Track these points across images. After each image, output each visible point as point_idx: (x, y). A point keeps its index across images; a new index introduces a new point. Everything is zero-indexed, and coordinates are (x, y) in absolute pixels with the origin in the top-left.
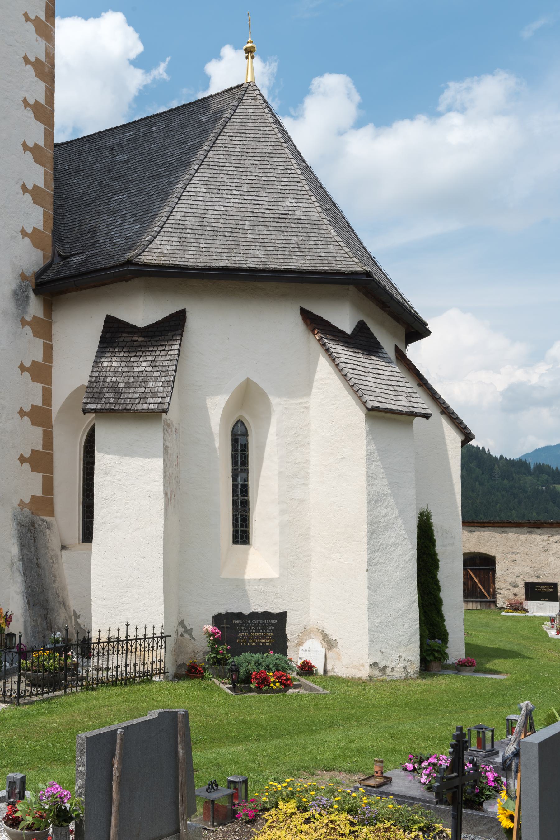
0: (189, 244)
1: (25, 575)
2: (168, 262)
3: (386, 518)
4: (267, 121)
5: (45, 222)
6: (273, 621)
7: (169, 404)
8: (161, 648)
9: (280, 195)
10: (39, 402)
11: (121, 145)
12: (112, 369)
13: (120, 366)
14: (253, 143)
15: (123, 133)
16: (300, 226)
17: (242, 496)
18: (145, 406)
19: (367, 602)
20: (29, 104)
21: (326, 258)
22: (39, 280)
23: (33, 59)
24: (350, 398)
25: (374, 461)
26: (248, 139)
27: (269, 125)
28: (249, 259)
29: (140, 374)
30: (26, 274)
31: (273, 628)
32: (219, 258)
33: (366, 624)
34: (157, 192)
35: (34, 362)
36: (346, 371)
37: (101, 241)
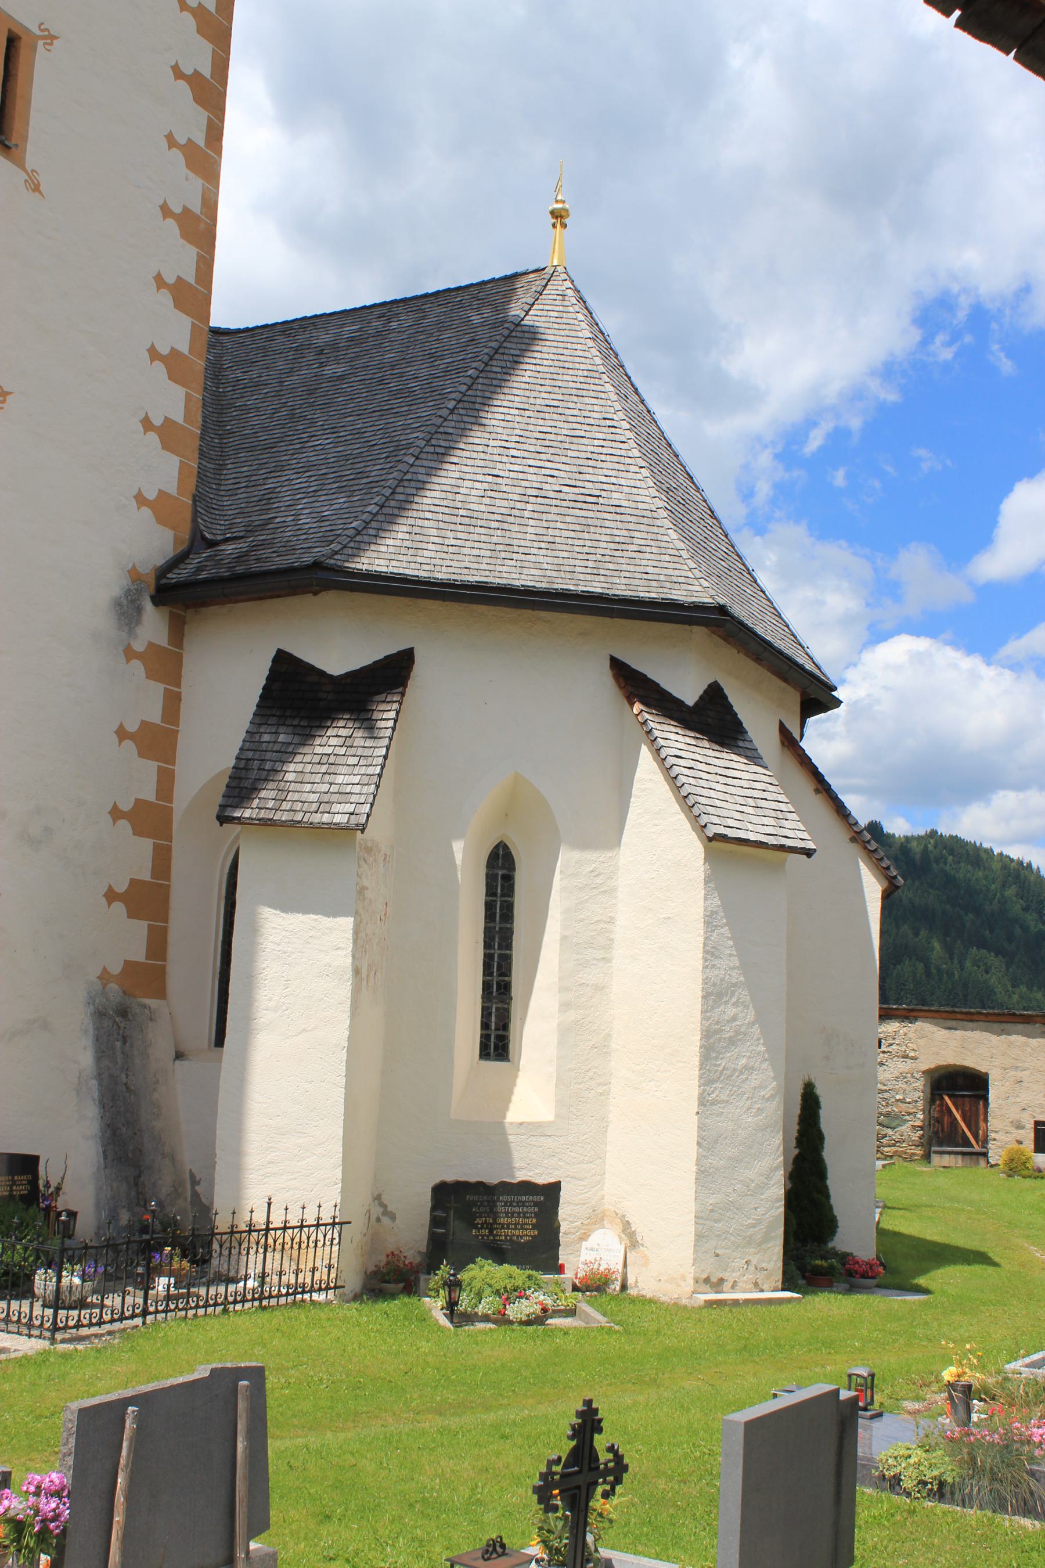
0: (425, 539)
1: (103, 1105)
2: (384, 569)
3: (734, 1024)
4: (580, 334)
5: (180, 481)
6: (537, 1198)
7: (368, 816)
8: (332, 1244)
9: (590, 463)
10: (149, 794)
11: (334, 347)
12: (277, 747)
13: (291, 744)
14: (552, 370)
15: (342, 326)
16: (618, 517)
17: (500, 975)
18: (326, 818)
19: (694, 1168)
20: (165, 283)
21: (656, 577)
22: (164, 581)
23: (178, 210)
24: (682, 816)
25: (716, 926)
26: (545, 362)
27: (582, 341)
28: (525, 571)
29: (325, 759)
30: (141, 570)
31: (536, 1209)
32: (476, 566)
33: (691, 1207)
34: (382, 441)
35: (144, 724)
36: (676, 770)
37: (278, 520)
